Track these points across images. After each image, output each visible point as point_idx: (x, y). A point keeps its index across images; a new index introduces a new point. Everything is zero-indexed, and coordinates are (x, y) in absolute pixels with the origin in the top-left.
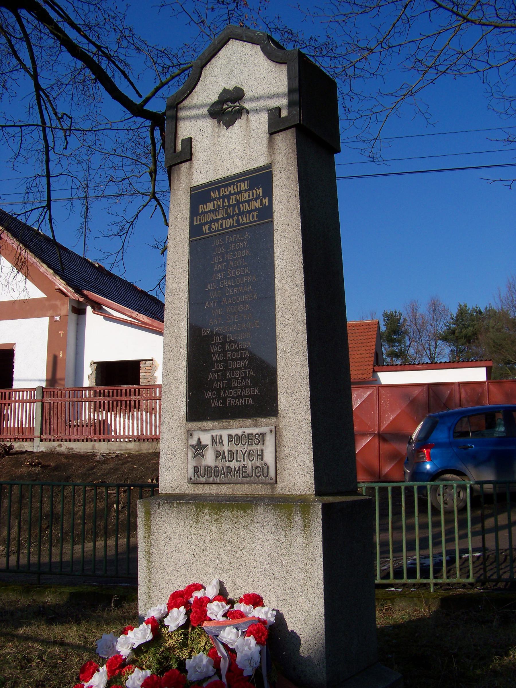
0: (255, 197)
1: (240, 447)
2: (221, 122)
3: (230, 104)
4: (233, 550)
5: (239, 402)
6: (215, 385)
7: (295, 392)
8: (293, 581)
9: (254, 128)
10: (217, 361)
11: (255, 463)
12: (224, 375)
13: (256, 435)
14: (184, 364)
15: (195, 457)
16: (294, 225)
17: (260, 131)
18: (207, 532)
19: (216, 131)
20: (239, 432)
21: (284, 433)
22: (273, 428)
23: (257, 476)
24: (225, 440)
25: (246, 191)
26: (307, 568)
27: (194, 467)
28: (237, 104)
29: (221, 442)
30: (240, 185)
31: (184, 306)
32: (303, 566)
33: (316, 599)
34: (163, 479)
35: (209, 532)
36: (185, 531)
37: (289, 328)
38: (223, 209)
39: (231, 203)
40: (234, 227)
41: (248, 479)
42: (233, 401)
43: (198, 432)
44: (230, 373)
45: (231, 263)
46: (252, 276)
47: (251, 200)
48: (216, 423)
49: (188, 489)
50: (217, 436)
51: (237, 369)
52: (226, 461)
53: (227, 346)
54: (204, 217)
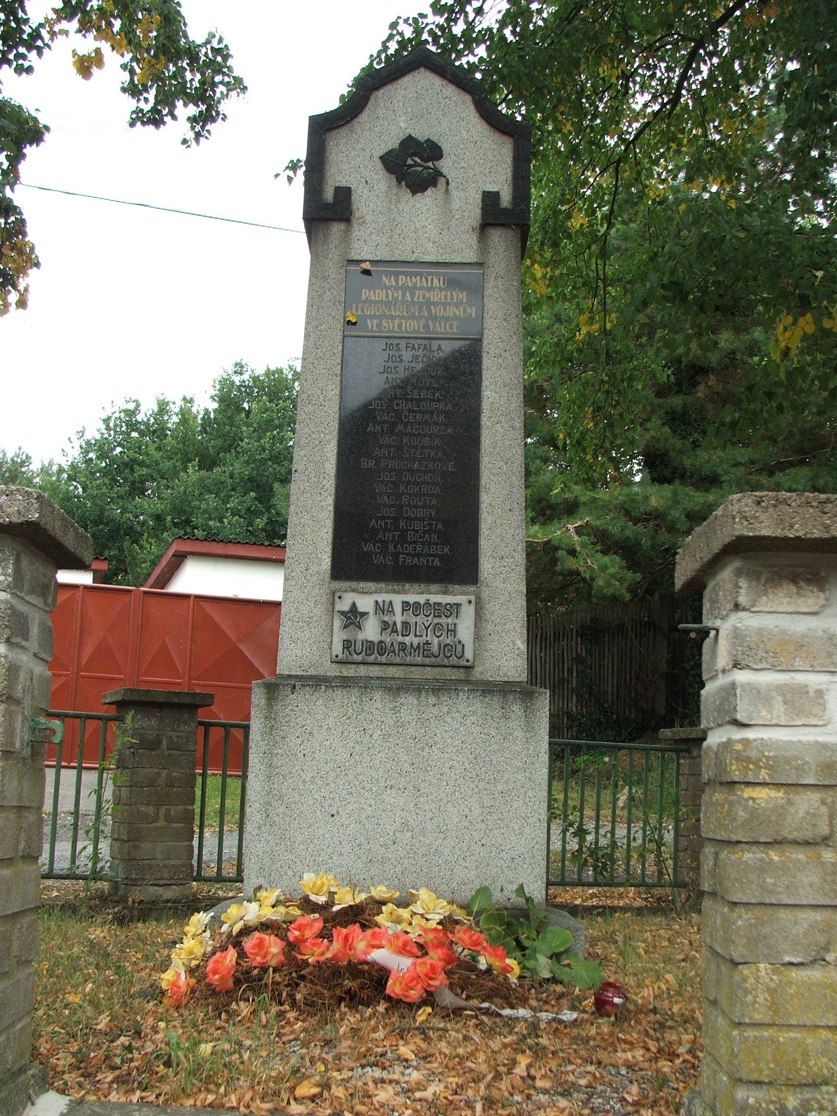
2: (403, 183)
3: (419, 161)
4: (418, 746)
6: (380, 535)
8: (506, 783)
9: (457, 207)
10: (385, 505)
15: (345, 627)
17: (466, 214)
19: (395, 192)
20: (421, 599)
24: (398, 608)
25: (441, 289)
30: (432, 279)
32: (521, 764)
33: (537, 803)
37: (500, 479)
39: (416, 299)
41: (433, 659)
46: (446, 405)
47: (449, 304)
48: (382, 585)
49: (333, 671)
51: (416, 518)
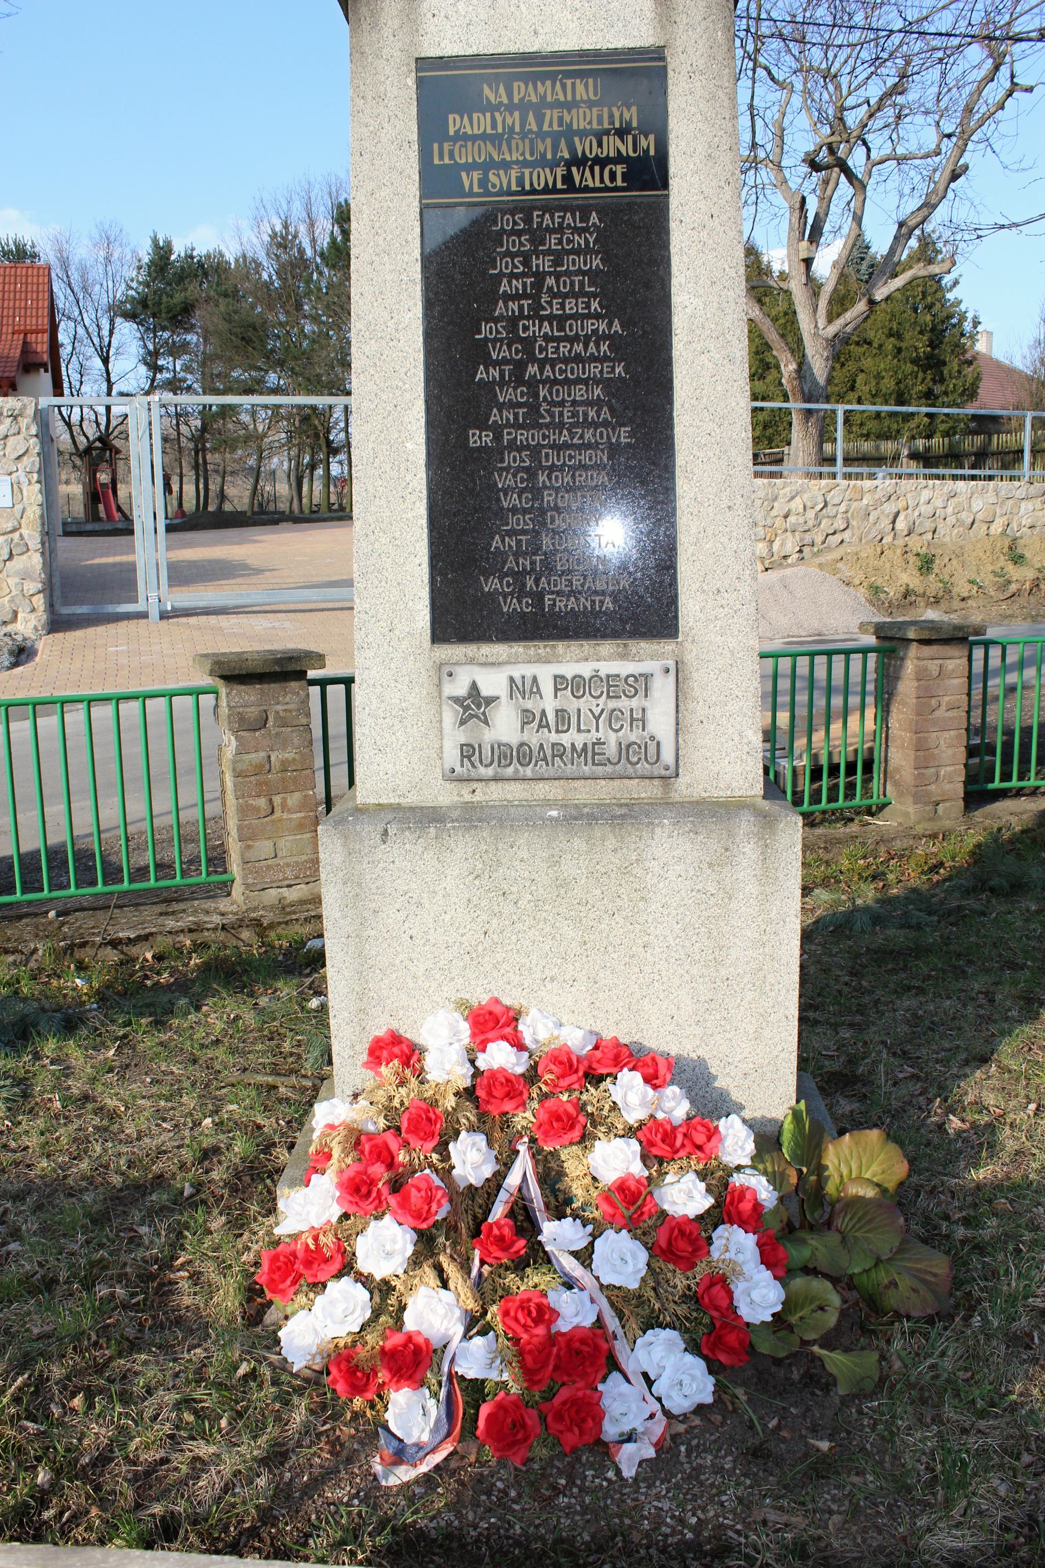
4: (591, 916)
6: (511, 563)
10: (514, 510)
13: (628, 676)
15: (463, 722)
16: (724, 218)
20: (586, 670)
21: (695, 675)
24: (547, 686)
25: (591, 104)
26: (765, 938)
27: (462, 745)
31: (413, 371)
38: (523, 139)
40: (555, 190)
41: (609, 769)
45: (550, 281)
47: (607, 133)
48: (518, 649)
53: (542, 478)
54: (463, 150)
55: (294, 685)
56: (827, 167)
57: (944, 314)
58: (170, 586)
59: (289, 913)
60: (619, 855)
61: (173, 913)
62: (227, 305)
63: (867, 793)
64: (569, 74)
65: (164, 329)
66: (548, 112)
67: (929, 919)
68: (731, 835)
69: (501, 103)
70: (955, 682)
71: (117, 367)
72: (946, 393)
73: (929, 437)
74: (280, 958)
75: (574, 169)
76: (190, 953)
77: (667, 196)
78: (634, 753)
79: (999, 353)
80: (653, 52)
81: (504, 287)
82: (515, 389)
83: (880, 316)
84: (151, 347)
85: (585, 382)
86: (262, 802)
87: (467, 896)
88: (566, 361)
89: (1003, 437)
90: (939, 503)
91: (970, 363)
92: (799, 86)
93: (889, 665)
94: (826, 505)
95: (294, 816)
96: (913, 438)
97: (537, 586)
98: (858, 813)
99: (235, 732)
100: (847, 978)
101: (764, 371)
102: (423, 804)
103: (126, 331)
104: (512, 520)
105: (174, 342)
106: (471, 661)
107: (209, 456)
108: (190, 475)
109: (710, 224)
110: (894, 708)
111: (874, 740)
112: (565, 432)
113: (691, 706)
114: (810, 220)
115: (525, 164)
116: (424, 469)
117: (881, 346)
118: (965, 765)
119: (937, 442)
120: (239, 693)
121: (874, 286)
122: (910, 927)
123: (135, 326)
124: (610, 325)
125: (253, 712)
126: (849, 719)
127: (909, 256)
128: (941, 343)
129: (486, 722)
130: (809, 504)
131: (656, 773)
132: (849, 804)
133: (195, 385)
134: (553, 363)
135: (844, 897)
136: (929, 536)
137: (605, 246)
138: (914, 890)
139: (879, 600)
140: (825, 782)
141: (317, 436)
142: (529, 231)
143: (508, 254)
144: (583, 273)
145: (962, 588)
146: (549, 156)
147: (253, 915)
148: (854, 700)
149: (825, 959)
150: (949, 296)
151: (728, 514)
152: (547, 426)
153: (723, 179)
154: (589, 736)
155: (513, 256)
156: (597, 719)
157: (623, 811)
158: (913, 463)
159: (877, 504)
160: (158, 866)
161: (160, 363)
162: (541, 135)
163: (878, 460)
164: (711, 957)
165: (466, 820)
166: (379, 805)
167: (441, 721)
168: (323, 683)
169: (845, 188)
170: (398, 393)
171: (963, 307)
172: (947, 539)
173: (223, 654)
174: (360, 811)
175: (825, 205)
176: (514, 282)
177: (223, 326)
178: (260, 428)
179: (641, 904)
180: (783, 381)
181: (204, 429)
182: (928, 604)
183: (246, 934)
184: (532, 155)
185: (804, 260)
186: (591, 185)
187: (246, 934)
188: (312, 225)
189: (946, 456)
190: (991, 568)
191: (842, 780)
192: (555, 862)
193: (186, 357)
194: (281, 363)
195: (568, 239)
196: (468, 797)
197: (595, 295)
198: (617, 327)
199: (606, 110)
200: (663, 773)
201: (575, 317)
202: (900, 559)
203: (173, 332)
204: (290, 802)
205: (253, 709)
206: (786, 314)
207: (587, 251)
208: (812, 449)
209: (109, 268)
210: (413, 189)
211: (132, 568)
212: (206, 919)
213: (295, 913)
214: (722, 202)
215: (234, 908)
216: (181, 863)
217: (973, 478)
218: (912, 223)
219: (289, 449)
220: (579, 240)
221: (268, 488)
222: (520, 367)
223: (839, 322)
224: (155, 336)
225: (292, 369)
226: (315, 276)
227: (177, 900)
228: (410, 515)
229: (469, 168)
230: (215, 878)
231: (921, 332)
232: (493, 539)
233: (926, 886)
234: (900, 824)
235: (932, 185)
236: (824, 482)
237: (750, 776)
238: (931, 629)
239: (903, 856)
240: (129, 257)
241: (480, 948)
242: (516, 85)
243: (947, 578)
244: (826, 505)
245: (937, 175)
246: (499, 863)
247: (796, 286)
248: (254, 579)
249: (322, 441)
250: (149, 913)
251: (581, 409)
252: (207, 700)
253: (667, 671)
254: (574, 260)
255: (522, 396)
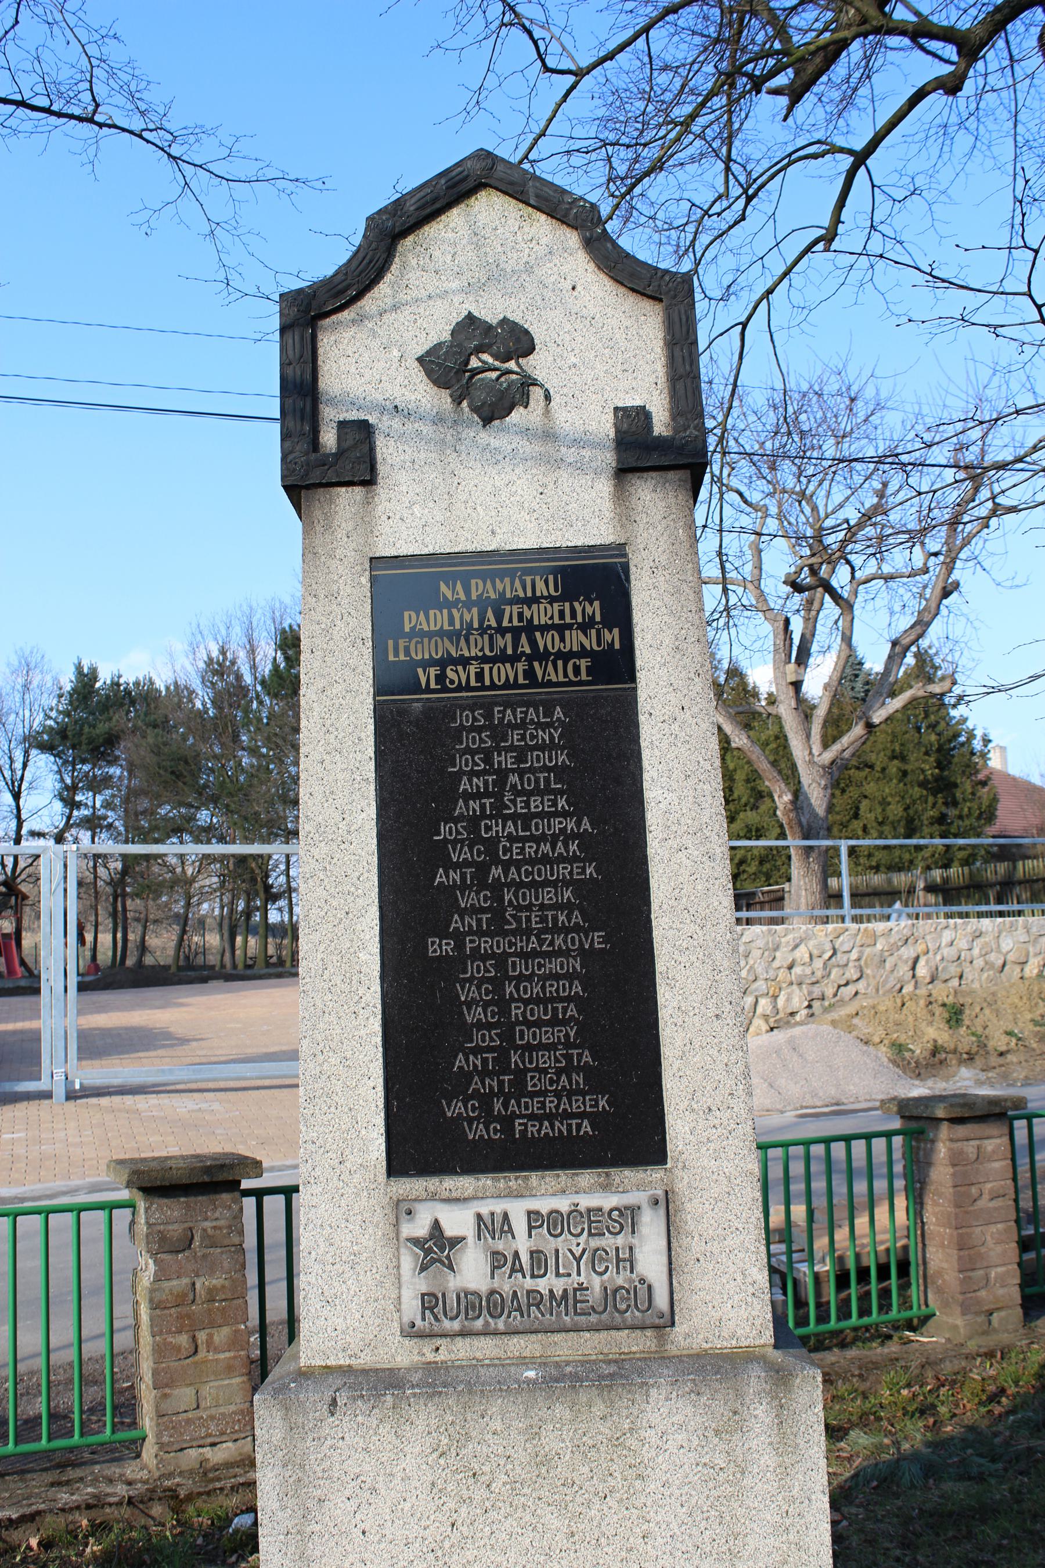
0: (580, 619)
1: (566, 1240)
4: (579, 1499)
5: (553, 1129)
6: (476, 1083)
7: (714, 1108)
10: (479, 1025)
11: (611, 1279)
12: (503, 1060)
13: (612, 1210)
14: (376, 1025)
15: (423, 1268)
16: (695, 709)
18: (495, 1465)
20: (563, 1205)
21: (688, 1206)
22: (660, 1192)
23: (618, 1310)
24: (519, 1225)
25: (552, 600)
26: (788, 1522)
27: (423, 1295)
28: (512, 365)
29: (506, 1228)
31: (366, 875)
32: (778, 1518)
34: (313, 1329)
35: (502, 1463)
36: (424, 1467)
37: (693, 958)
38: (481, 635)
40: (516, 685)
41: (593, 1318)
42: (533, 1126)
43: (430, 1204)
44: (522, 1056)
45: (514, 779)
47: (569, 627)
48: (486, 1181)
50: (492, 1214)
51: (541, 1046)
52: (524, 1277)
53: (510, 989)
54: (419, 646)
55: (226, 1197)
56: (809, 588)
57: (951, 733)
58: (79, 1059)
59: (212, 1480)
60: (609, 1424)
61: (68, 1483)
62: (157, 735)
63: (905, 1303)
64: (527, 572)
65: (84, 761)
66: (508, 608)
67: (993, 1467)
68: (739, 1395)
69: (458, 600)
70: (997, 1165)
71: (28, 802)
72: (960, 817)
73: (946, 866)
74: (200, 1541)
75: (536, 664)
76: (86, 1537)
77: (635, 689)
78: (622, 1299)
79: (1015, 769)
80: (613, 549)
81: (464, 785)
82: (478, 893)
83: (881, 737)
84: (69, 781)
85: (554, 884)
86: (183, 1340)
87: (430, 1479)
88: (532, 862)
89: (1029, 863)
90: (963, 944)
91: (984, 783)
92: (773, 510)
93: (918, 1148)
94: (834, 953)
95: (222, 1356)
96: (928, 868)
97: (506, 1109)
98: (896, 1328)
99: (153, 1255)
100: (898, 1552)
101: (757, 800)
102: (378, 1366)
103: (42, 764)
104: (477, 1036)
105: (95, 776)
106: (433, 1197)
107: (129, 902)
108: (106, 922)
109: (680, 716)
110: (928, 1201)
111: (908, 1237)
112: (533, 938)
113: (686, 1241)
114: (796, 641)
115: (485, 660)
116: (378, 981)
117: (884, 769)
118: (1019, 1265)
119: (955, 872)
120: (160, 1208)
121: (870, 708)
122: (970, 1478)
123: (52, 758)
124: (579, 824)
125: (176, 1230)
126: (877, 1211)
127: (905, 673)
128: (950, 763)
129: (451, 1267)
130: (815, 952)
131: (648, 1322)
132: (884, 1318)
133: (117, 823)
134: (518, 865)
135: (886, 1441)
136: (955, 982)
137: (570, 741)
138: (971, 1428)
139: (904, 1059)
140: (853, 1291)
141: (253, 880)
142: (490, 727)
143: (468, 750)
144: (549, 769)
145: (999, 1041)
146: (510, 651)
147: (168, 1483)
148: (880, 1185)
149: (870, 1526)
150: (953, 713)
151: (716, 1023)
152: (513, 932)
153: (693, 671)
154: (569, 1280)
155: (473, 753)
156: (578, 1260)
157: (613, 1368)
158: (931, 898)
159: (894, 948)
160: (53, 1416)
161: (78, 798)
162: (502, 631)
163: (887, 896)
164: (724, 1548)
165: (429, 1385)
166: (327, 1367)
167: (398, 1267)
168: (259, 1194)
169: (830, 609)
170: (350, 899)
171: (970, 724)
172: (976, 985)
173: (144, 1160)
174: (304, 1375)
175: (810, 626)
176: (475, 780)
177: (151, 759)
178: (189, 871)
179: (638, 1484)
180: (778, 813)
181: (125, 872)
182: (961, 1062)
183: (157, 1510)
184: (491, 651)
185: (792, 683)
186: (554, 680)
187: (157, 1510)
188: (252, 651)
189: (968, 887)
190: (1029, 1016)
191: (874, 1286)
192: (533, 1434)
193: (108, 792)
194: (215, 800)
195: (531, 734)
196: (430, 1356)
197: (561, 792)
198: (586, 824)
199: (567, 605)
200: (657, 1321)
201: (541, 815)
202: (925, 1011)
203: (94, 767)
204: (216, 1339)
205: (175, 1227)
206: (777, 738)
207: (552, 746)
208: (816, 887)
209: (27, 696)
210: (367, 686)
211: (35, 1037)
212: (109, 1490)
213: (219, 1479)
214: (692, 694)
215: (144, 1474)
216: (82, 1412)
217: (1001, 914)
218: (906, 641)
219: (222, 894)
220: (543, 736)
221: (196, 939)
222: (482, 870)
223: (836, 747)
224: (74, 770)
225: (227, 806)
226: (255, 705)
227: (74, 1465)
228: (362, 1032)
229: (426, 664)
230: (121, 1435)
231: (927, 753)
232: (456, 1057)
233: (986, 1422)
234: (948, 1340)
235: (924, 603)
236: (830, 927)
237: (758, 1322)
238: (964, 1105)
239: (954, 1382)
240: (49, 685)
241: (447, 1544)
242: (473, 582)
243: (979, 1030)
244: (834, 953)
245: (928, 591)
246: (468, 1437)
247: (786, 710)
248: (179, 1051)
249: (260, 886)
250: (37, 1482)
251: (550, 913)
252: (122, 1216)
253: (656, 1202)
254: (538, 756)
255: (485, 901)
